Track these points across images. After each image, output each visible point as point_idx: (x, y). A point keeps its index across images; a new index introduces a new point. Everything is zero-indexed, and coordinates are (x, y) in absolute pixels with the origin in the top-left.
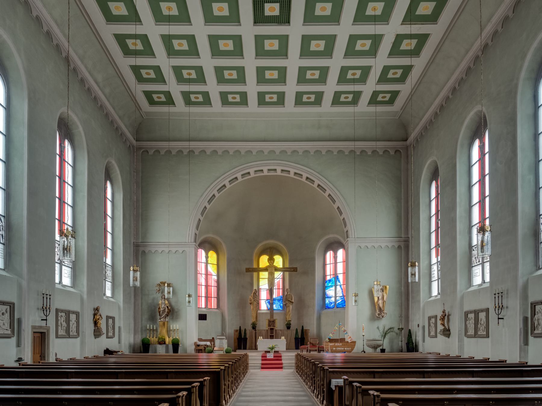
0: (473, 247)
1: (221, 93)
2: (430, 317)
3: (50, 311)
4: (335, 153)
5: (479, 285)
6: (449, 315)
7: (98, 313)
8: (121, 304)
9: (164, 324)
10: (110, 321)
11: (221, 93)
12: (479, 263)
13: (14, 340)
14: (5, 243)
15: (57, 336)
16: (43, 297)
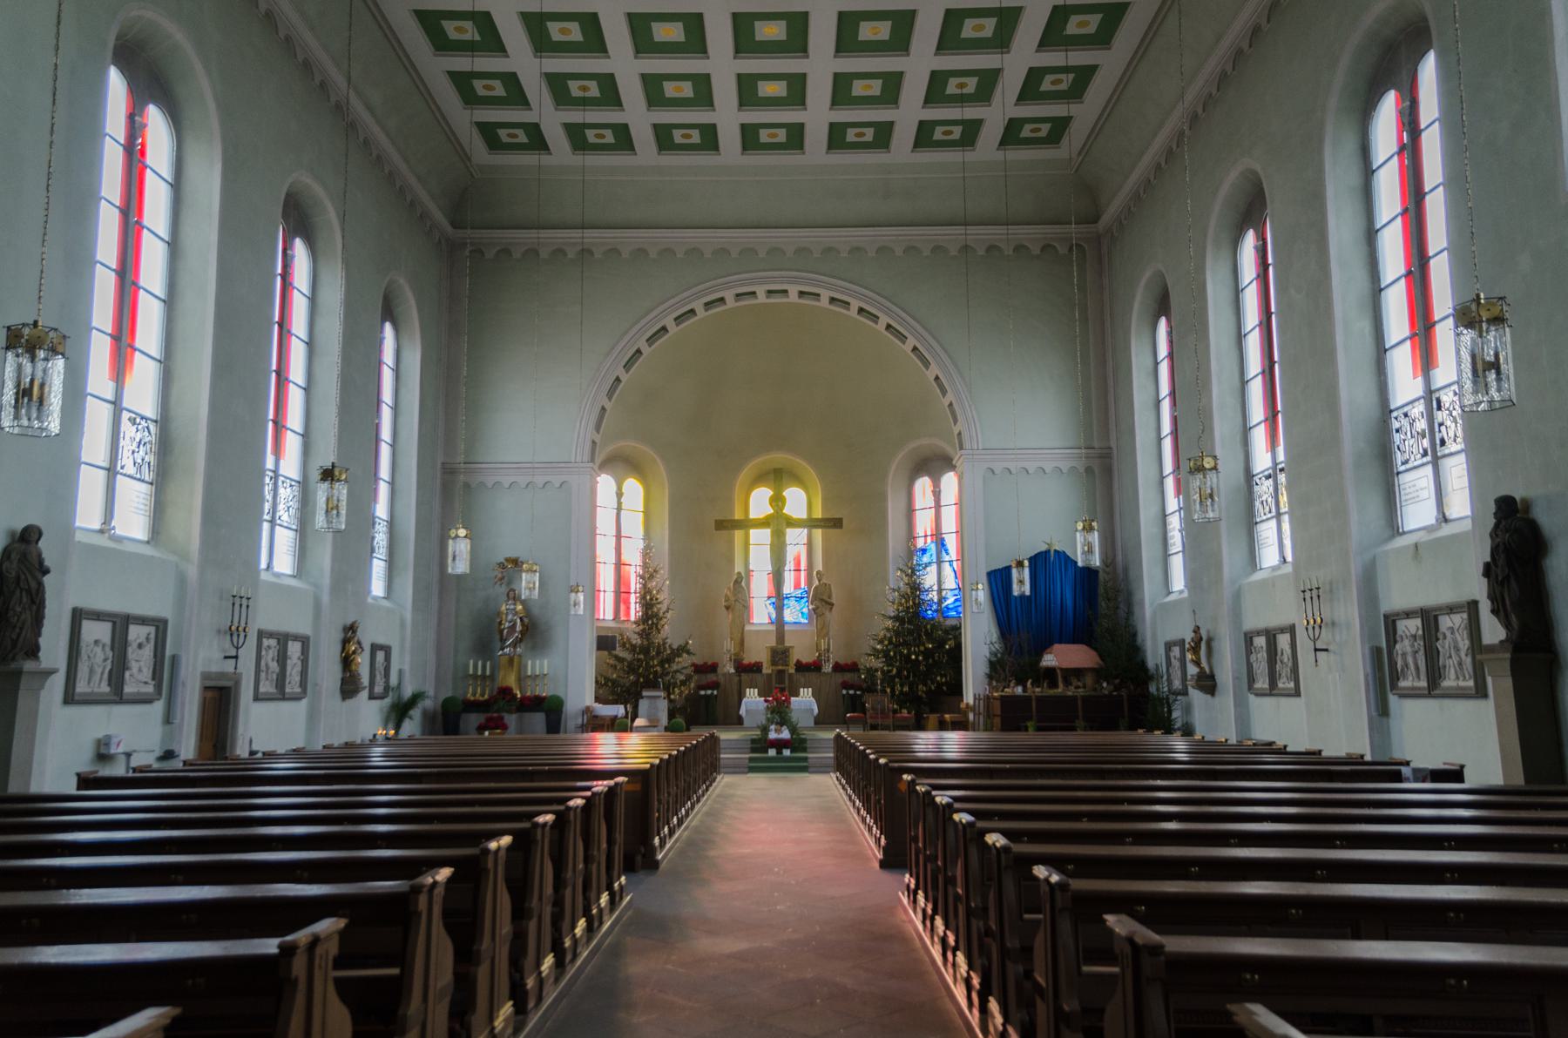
0: (1253, 476)
1: (656, 127)
2: (1252, 632)
3: (245, 636)
4: (926, 253)
5: (1274, 569)
6: (1209, 641)
7: (354, 637)
8: (408, 616)
9: (511, 661)
10: (380, 656)
11: (656, 127)
12: (1269, 516)
13: (159, 706)
14: (154, 482)
15: (257, 698)
16: (234, 604)
